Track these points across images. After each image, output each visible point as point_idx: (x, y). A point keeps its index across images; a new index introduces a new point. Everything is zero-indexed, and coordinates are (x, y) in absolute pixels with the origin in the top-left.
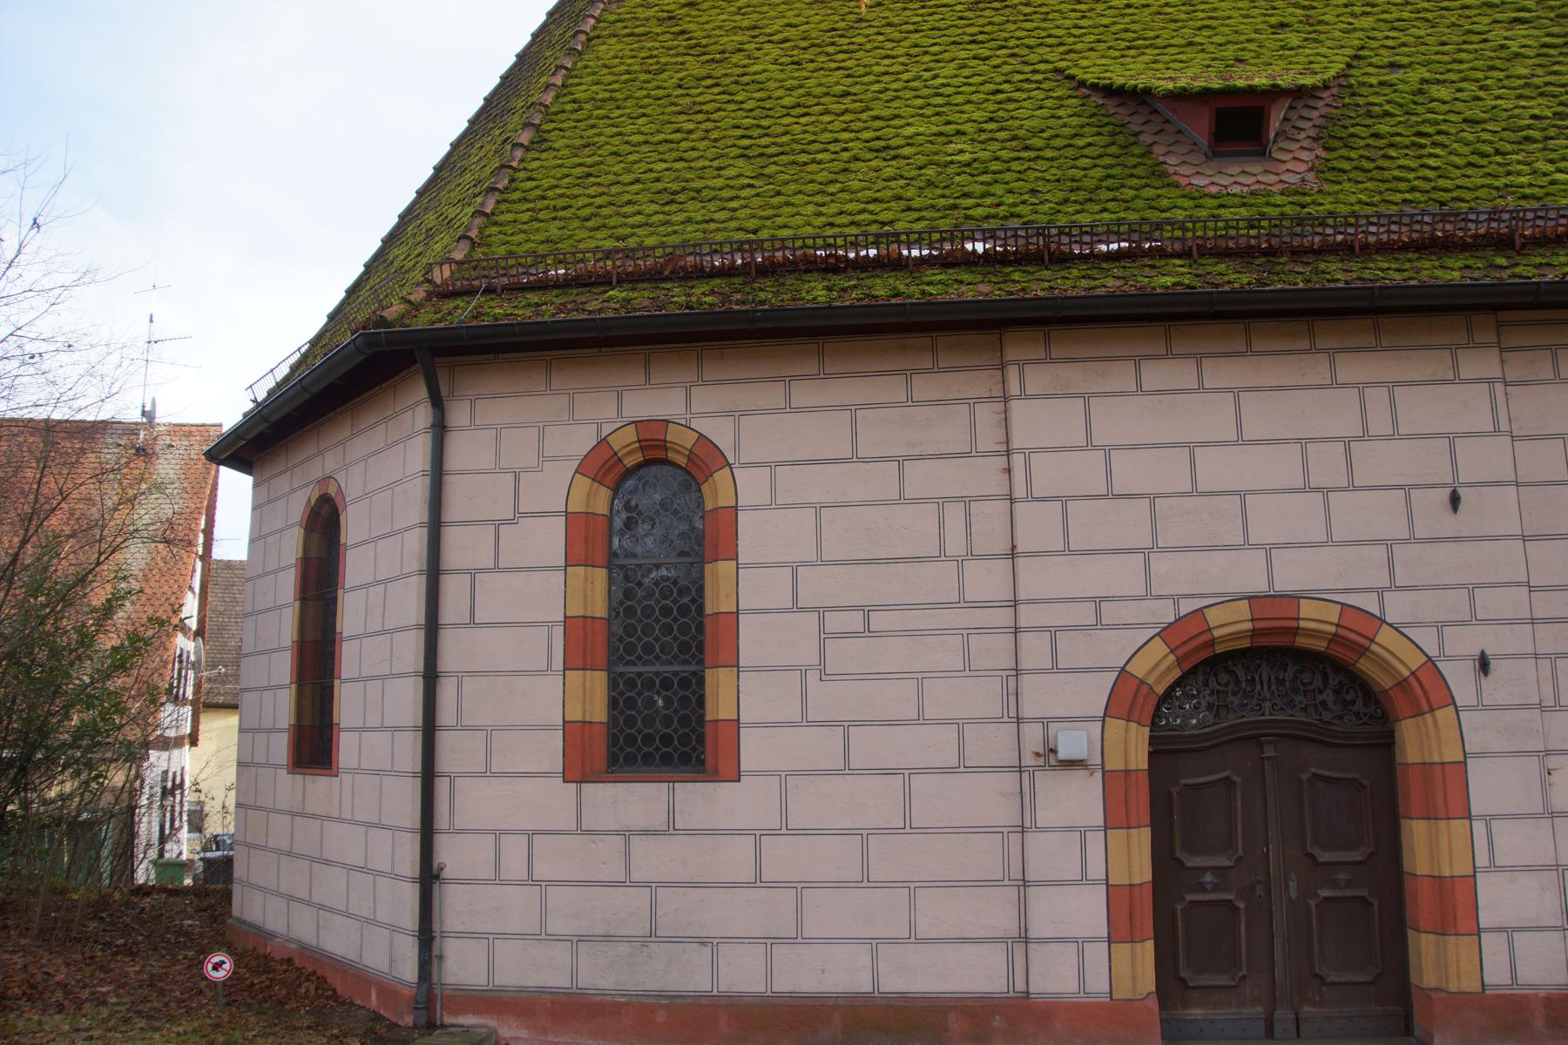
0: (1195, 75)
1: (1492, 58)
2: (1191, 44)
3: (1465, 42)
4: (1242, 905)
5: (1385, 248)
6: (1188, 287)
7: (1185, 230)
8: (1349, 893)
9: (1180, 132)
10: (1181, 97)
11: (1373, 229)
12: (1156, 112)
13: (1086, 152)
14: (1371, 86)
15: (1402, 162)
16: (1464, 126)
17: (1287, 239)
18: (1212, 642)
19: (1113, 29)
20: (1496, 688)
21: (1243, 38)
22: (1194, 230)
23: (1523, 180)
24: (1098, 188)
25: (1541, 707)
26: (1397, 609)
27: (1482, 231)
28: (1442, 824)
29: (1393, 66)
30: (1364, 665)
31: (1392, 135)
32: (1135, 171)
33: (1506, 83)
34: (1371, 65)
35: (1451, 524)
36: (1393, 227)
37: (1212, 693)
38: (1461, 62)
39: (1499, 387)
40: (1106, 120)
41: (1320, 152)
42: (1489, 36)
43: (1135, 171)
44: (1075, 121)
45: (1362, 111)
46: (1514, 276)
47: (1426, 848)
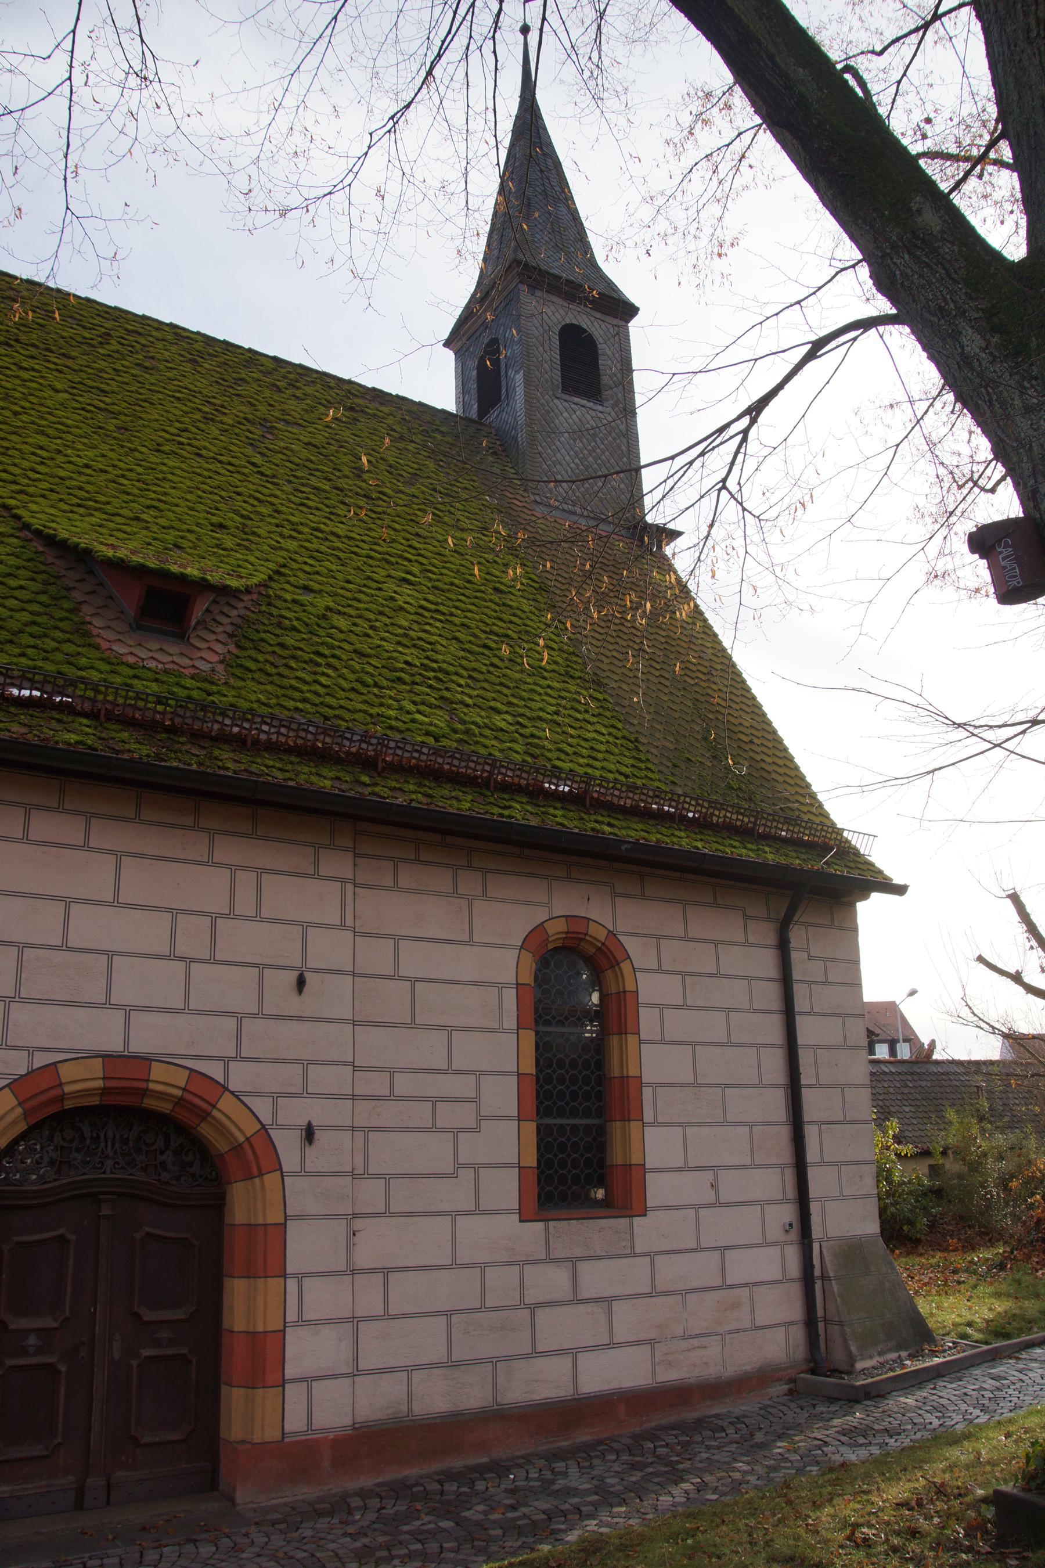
0: (132, 548)
1: (383, 605)
2: (137, 519)
3: (365, 586)
4: (63, 1368)
5: (272, 748)
6: (90, 748)
7: (97, 691)
8: (170, 1351)
9: (111, 597)
10: (118, 566)
11: (265, 728)
12: (91, 572)
13: (17, 593)
14: (286, 601)
15: (299, 674)
16: (354, 656)
17: (189, 721)
18: (62, 1098)
19: (68, 483)
20: (318, 1157)
21: (185, 527)
22: (106, 694)
23: (392, 713)
24: (21, 631)
25: (353, 1175)
26: (240, 1078)
27: (353, 750)
28: (260, 1282)
29: (307, 589)
30: (205, 1130)
31: (296, 648)
32: (61, 624)
33: (390, 628)
34: (288, 582)
35: (294, 1004)
36: (283, 730)
37: (56, 1148)
38: (359, 601)
39: (350, 887)
40: (43, 568)
41: (232, 648)
42: (384, 586)
43: (61, 624)
44: (12, 561)
45: (275, 620)
46: (373, 794)
47: (243, 1305)
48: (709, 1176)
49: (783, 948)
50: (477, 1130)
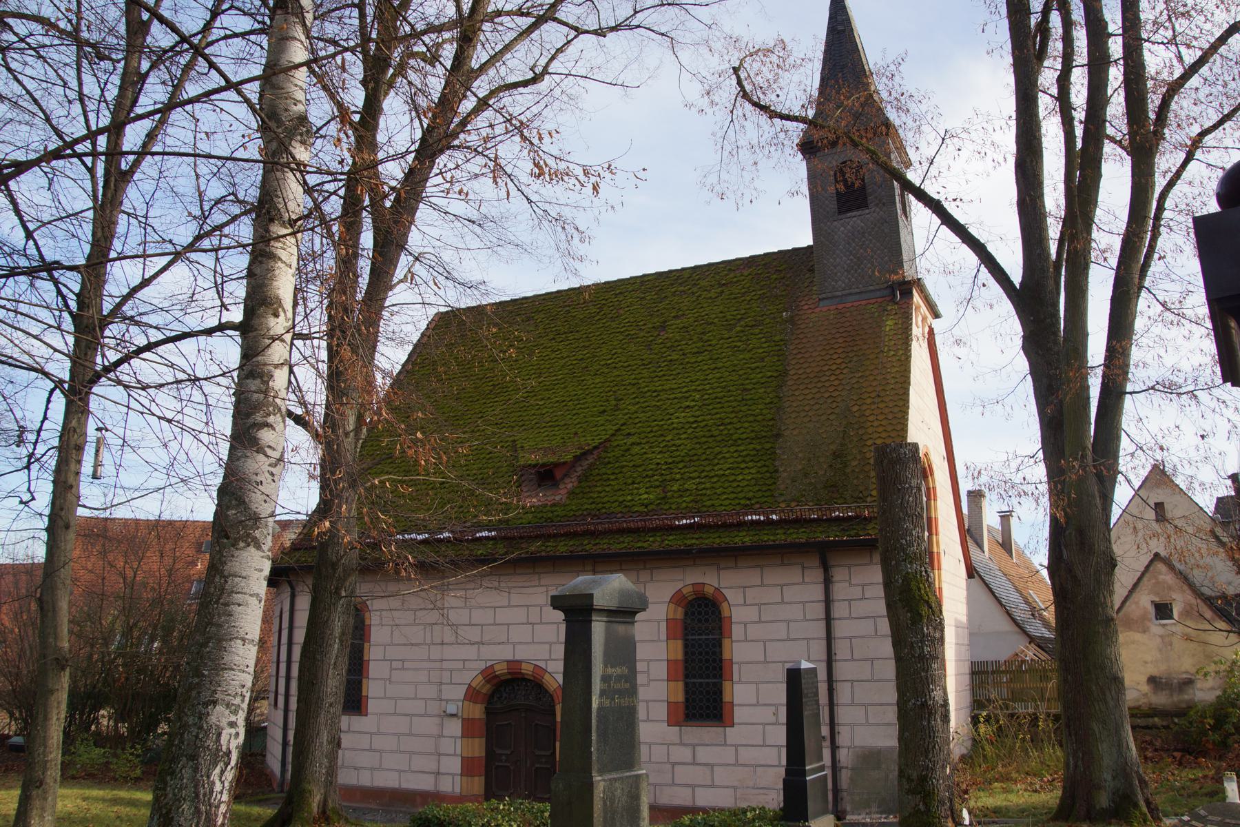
47: (477, 748)
48: (773, 708)
49: (828, 582)
50: (648, 685)
